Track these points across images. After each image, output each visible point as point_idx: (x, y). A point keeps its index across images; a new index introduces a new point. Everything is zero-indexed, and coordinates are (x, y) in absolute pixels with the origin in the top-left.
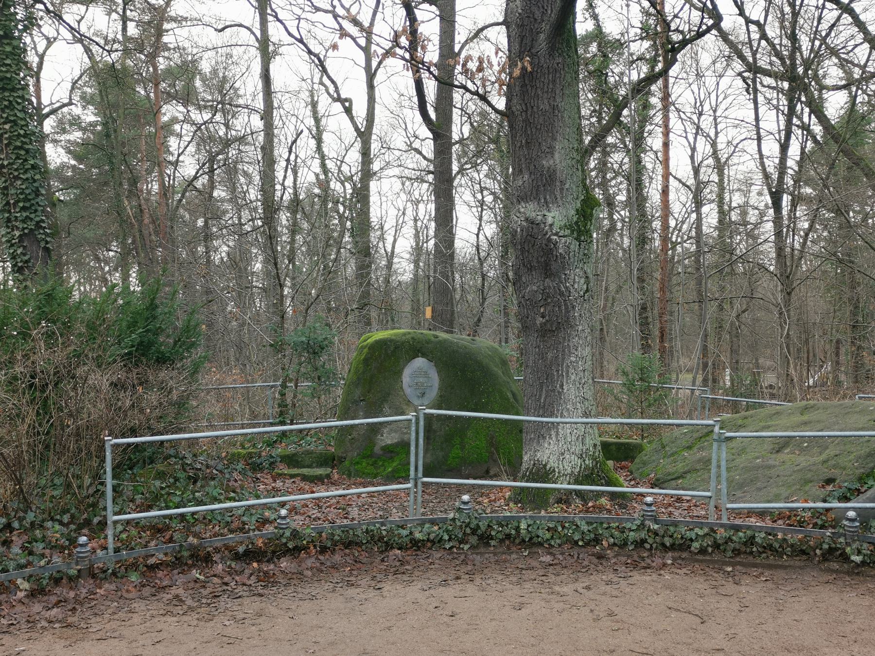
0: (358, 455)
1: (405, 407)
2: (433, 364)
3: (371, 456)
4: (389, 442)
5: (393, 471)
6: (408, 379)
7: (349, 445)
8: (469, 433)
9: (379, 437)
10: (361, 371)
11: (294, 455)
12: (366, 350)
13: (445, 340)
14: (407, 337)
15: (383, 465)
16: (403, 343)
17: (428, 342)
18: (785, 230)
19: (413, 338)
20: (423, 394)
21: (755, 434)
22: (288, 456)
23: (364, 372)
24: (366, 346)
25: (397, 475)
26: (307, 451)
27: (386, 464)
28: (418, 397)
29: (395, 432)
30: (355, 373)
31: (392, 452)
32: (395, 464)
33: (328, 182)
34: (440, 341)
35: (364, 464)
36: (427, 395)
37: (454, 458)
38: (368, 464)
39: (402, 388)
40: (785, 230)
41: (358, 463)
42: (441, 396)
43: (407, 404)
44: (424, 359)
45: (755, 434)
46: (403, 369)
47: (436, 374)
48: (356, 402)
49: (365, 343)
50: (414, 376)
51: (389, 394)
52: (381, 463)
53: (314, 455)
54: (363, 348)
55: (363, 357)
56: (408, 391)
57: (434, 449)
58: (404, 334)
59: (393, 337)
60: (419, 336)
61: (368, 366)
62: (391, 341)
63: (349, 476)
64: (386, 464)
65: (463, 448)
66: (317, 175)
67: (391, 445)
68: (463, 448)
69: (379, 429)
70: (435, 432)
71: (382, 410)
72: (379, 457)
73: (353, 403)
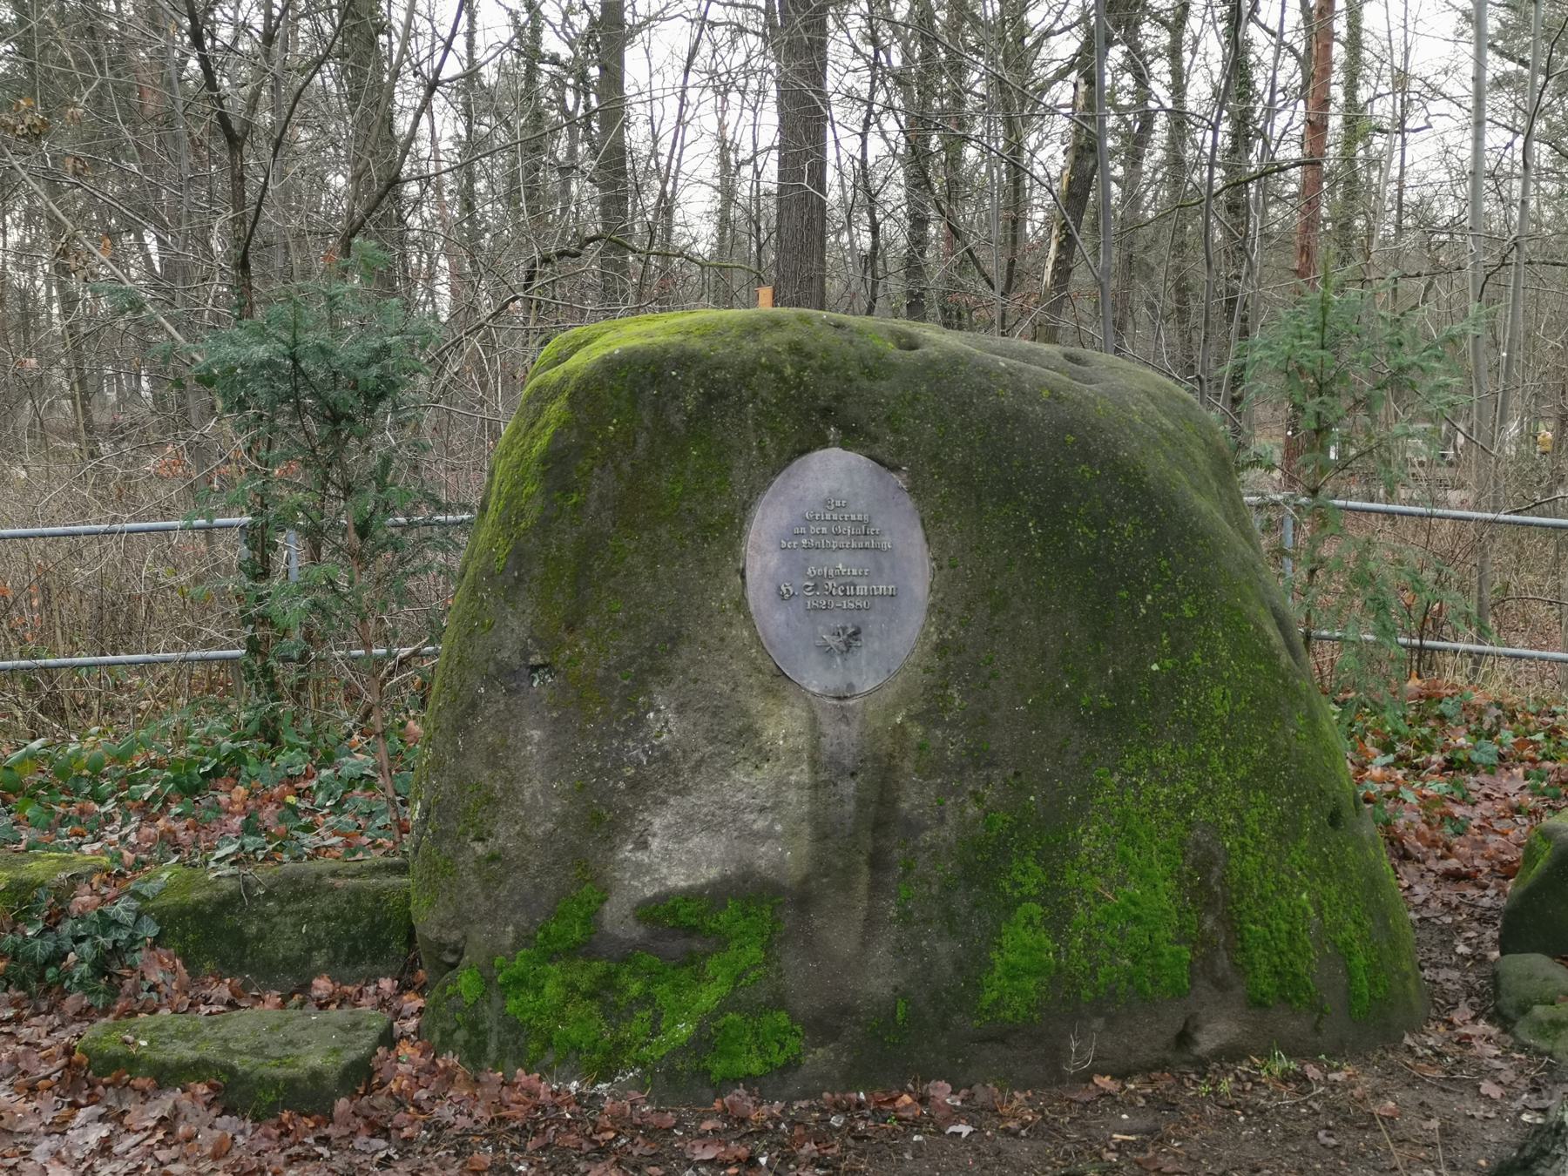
0: (523, 940)
1: (757, 705)
2: (898, 480)
3: (585, 950)
4: (678, 879)
5: (701, 1044)
6: (773, 560)
7: (475, 886)
8: (1088, 840)
9: (627, 851)
10: (533, 513)
11: (227, 903)
12: (556, 410)
13: (955, 361)
14: (768, 340)
15: (647, 1000)
16: (746, 372)
17: (875, 368)
18: (55, 293)
19: (796, 349)
20: (852, 638)
21: (1514, 517)
22: (195, 913)
23: (545, 525)
24: (557, 389)
25: (719, 1068)
26: (293, 881)
27: (662, 991)
28: (827, 651)
29: (711, 827)
30: (505, 523)
31: (691, 931)
32: (708, 997)
33: (536, 32)
34: (931, 364)
35: (551, 990)
36: (869, 645)
37: (1013, 973)
38: (572, 987)
39: (741, 605)
40: (55, 293)
41: (519, 982)
42: (941, 648)
43: (768, 691)
44: (854, 459)
45: (1514, 517)
46: (747, 507)
47: (918, 535)
48: (509, 677)
49: (555, 374)
50: (798, 542)
51: (675, 639)
52: (635, 988)
53: (324, 904)
54: (542, 396)
55: (541, 444)
56: (772, 619)
57: (905, 918)
58: (752, 330)
59: (696, 344)
60: (828, 336)
61: (567, 490)
62: (685, 360)
63: (475, 1054)
64: (662, 991)
65: (1058, 920)
66: (514, 15)
67: (690, 895)
68: (1058, 920)
69: (628, 813)
70: (912, 828)
71: (639, 721)
72: (626, 955)
73: (489, 680)
